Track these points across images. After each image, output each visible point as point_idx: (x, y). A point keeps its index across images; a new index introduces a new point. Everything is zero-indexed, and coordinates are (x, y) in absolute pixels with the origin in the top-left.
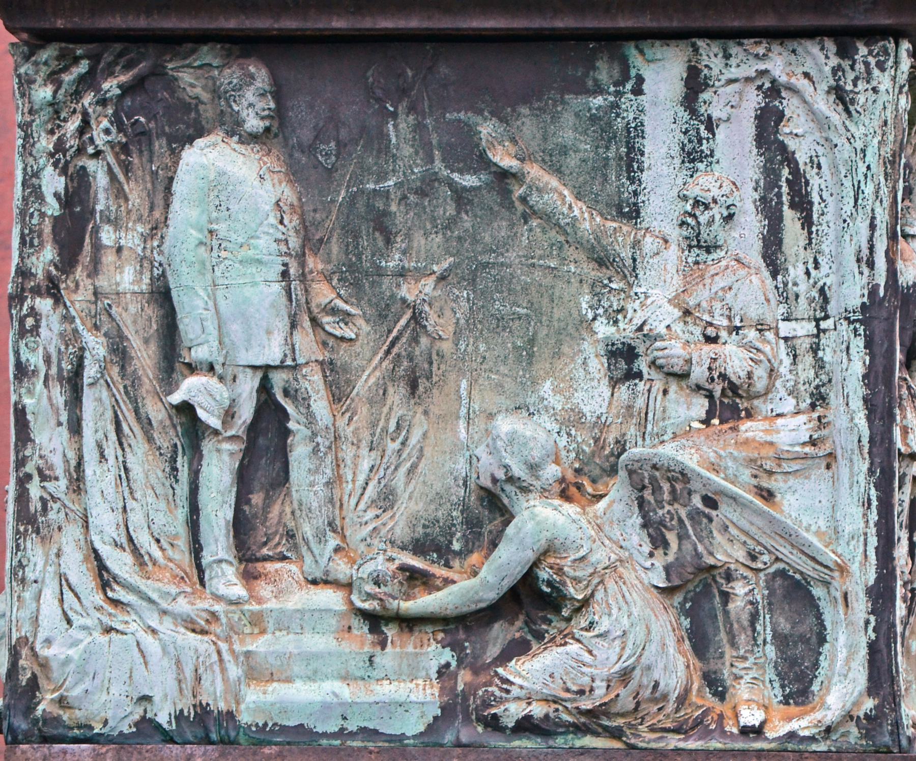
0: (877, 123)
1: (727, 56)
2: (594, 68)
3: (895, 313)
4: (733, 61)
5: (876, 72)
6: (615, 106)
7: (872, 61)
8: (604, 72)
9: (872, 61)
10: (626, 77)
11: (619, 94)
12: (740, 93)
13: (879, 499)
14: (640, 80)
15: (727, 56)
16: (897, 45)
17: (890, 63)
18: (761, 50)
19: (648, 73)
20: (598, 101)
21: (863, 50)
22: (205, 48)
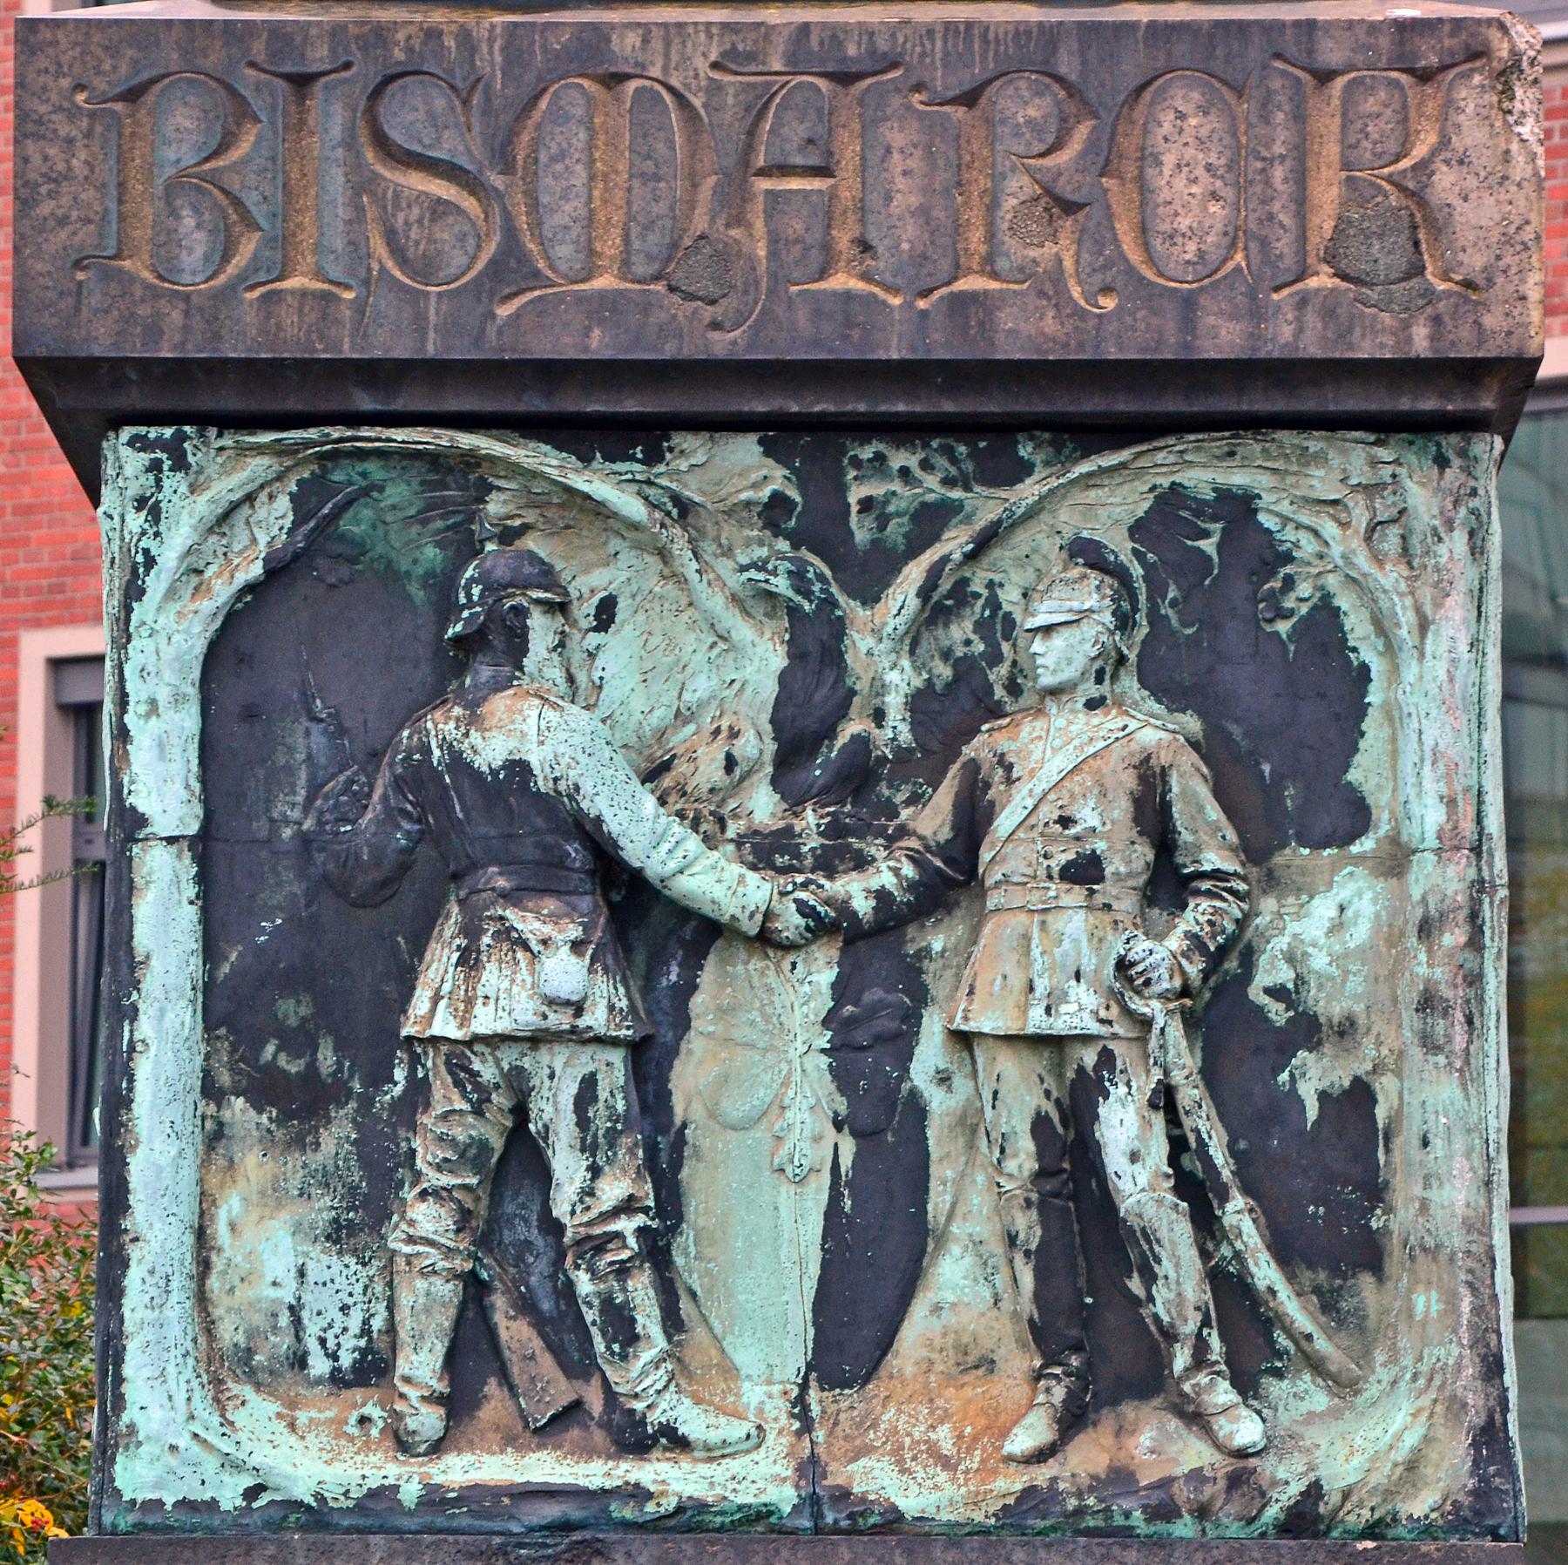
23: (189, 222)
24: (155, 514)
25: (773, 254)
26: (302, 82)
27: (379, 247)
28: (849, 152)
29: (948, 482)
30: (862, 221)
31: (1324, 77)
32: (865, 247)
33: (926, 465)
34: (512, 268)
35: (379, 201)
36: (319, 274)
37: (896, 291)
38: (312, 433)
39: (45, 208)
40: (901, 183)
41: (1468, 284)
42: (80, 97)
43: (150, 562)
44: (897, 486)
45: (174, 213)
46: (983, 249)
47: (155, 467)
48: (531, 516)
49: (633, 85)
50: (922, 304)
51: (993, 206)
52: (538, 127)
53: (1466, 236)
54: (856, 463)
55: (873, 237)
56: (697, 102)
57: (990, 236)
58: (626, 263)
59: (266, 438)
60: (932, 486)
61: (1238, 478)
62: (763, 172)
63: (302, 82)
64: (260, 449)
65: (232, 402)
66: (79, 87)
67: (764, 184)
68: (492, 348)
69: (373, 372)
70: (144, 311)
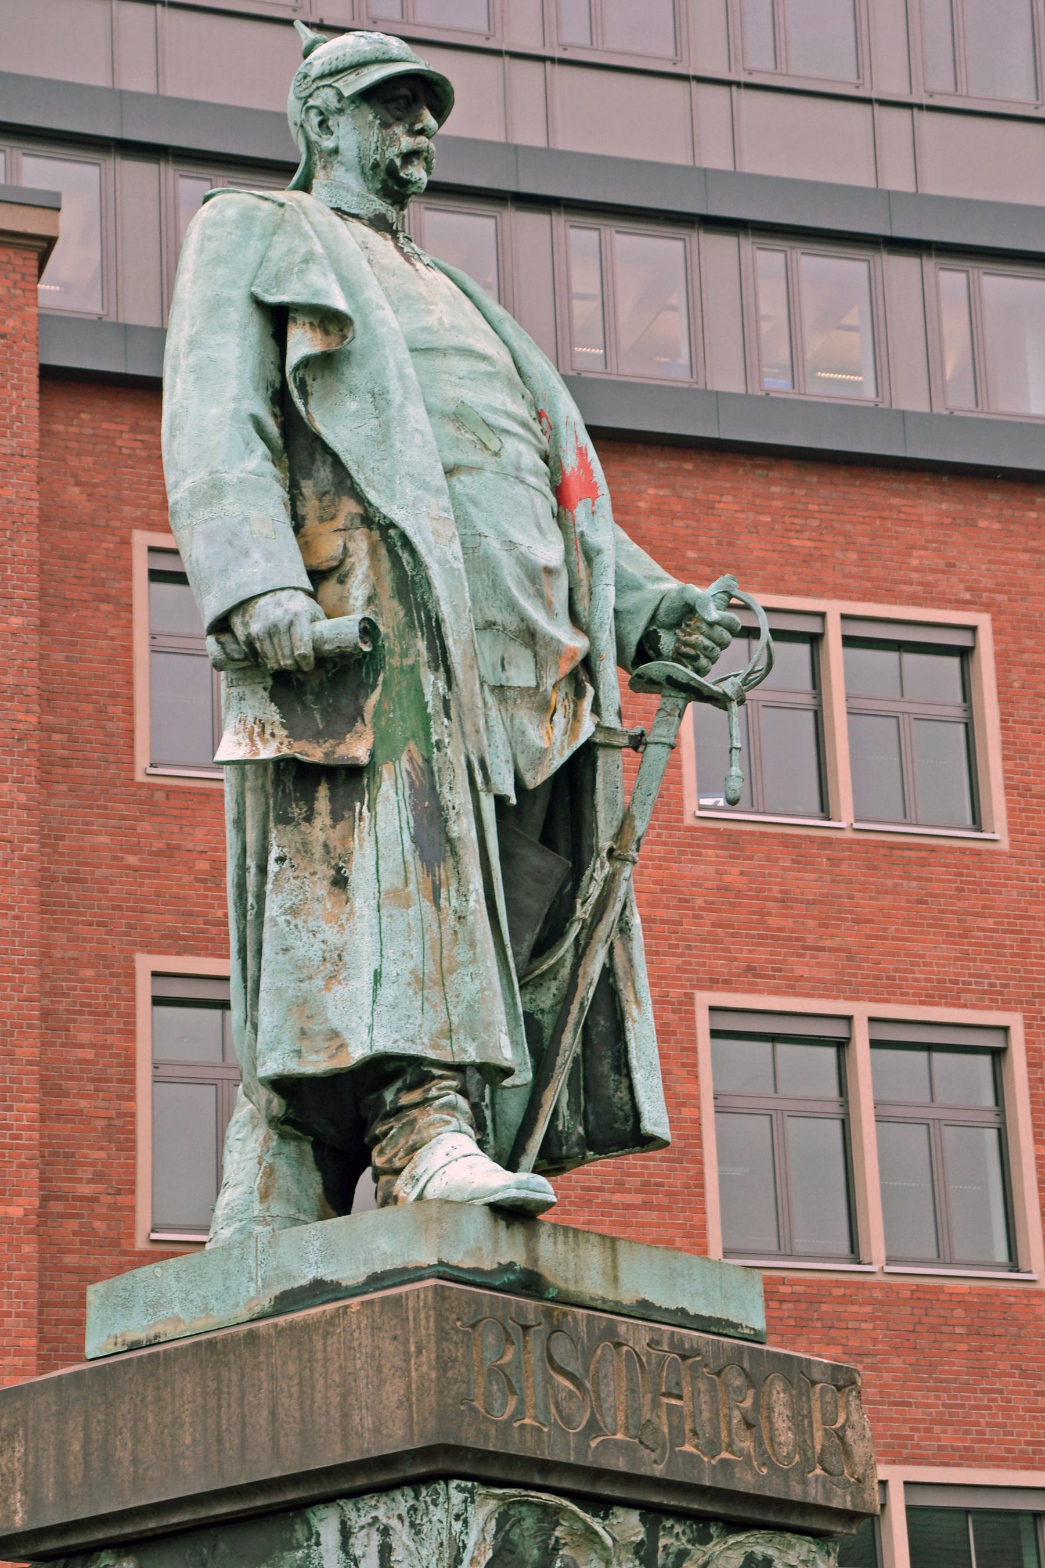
0: (434, 1546)
1: (358, 1510)
2: (294, 1530)
3: (820, 378)
4: (362, 1513)
5: (431, 1508)
6: (308, 1556)
7: (429, 1499)
8: (300, 1533)
9: (429, 1499)
10: (311, 1535)
11: (309, 1547)
12: (368, 1535)
13: (571, 1003)
14: (318, 1535)
15: (358, 1510)
16: (447, 1485)
17: (441, 1500)
18: (373, 1503)
19: (321, 1530)
20: (300, 1554)
21: (424, 1492)
22: (103, 1554)
23: (495, 1387)
24: (466, 1522)
25: (670, 1432)
26: (526, 1328)
27: (553, 1411)
28: (687, 1391)
29: (689, 1541)
30: (694, 1421)
31: (814, 1383)
32: (695, 1433)
33: (684, 1533)
34: (594, 1427)
35: (553, 1387)
36: (535, 1418)
37: (705, 1454)
38: (513, 1491)
39: (450, 1374)
40: (704, 1407)
41: (858, 1480)
42: (459, 1324)
43: (465, 1547)
44: (673, 1540)
45: (490, 1382)
46: (727, 1440)
47: (465, 1501)
48: (568, 1539)
49: (625, 1348)
50: (713, 1462)
51: (729, 1422)
52: (598, 1362)
53: (857, 1459)
54: (664, 1528)
55: (698, 1429)
56: (644, 1360)
57: (730, 1435)
58: (627, 1428)
59: (500, 1491)
60: (683, 1543)
61: (770, 1552)
62: (664, 1395)
63: (526, 1328)
64: (495, 1496)
65: (495, 1473)
66: (459, 1319)
67: (665, 1400)
68: (589, 1461)
69: (546, 1466)
70: (483, 1427)
